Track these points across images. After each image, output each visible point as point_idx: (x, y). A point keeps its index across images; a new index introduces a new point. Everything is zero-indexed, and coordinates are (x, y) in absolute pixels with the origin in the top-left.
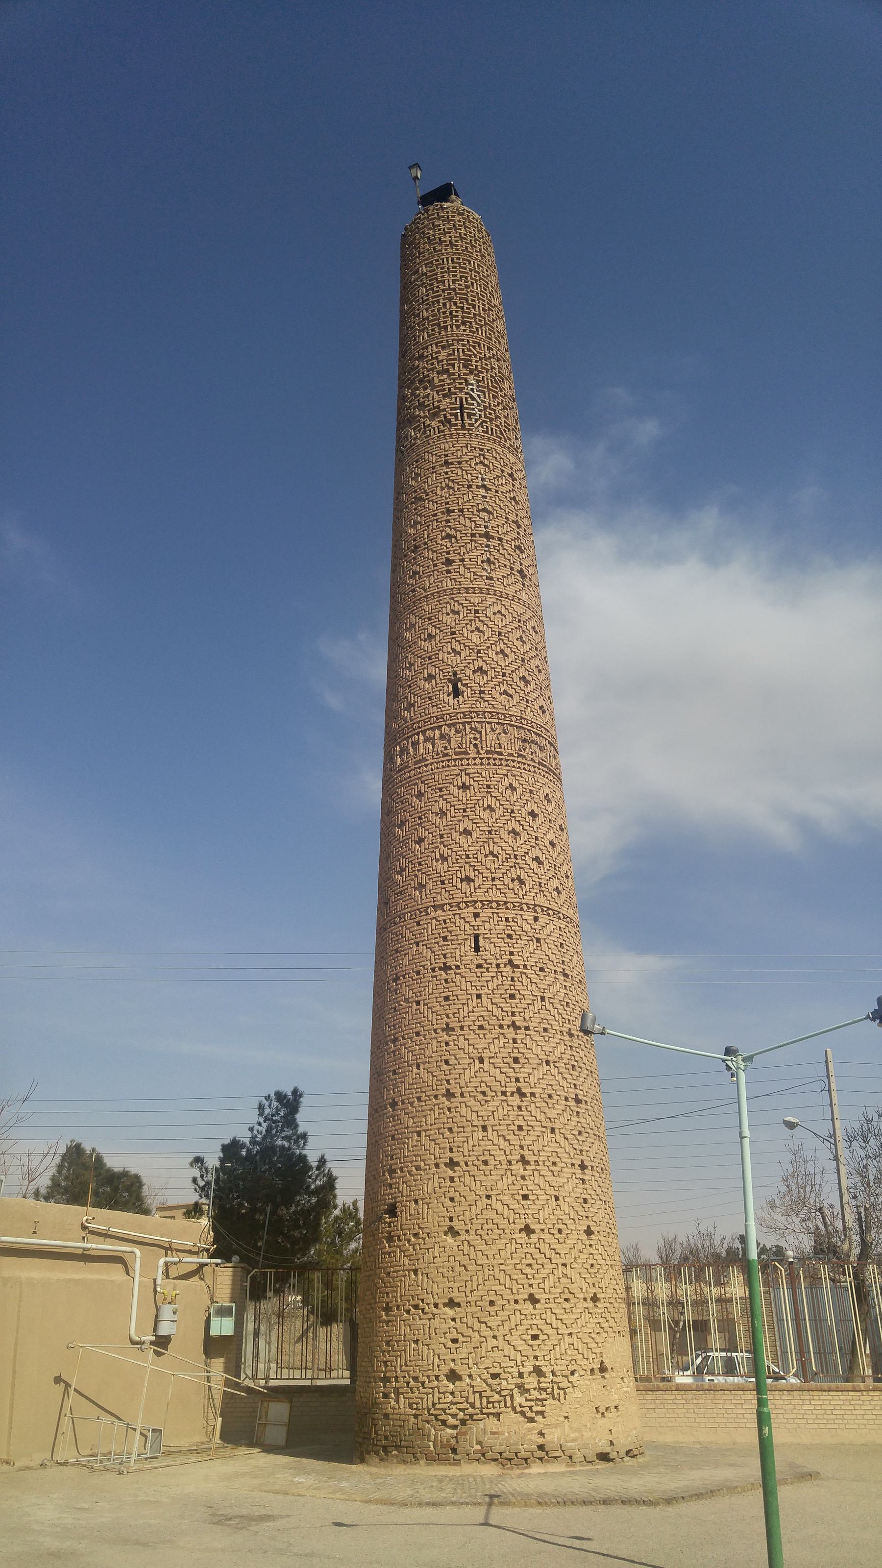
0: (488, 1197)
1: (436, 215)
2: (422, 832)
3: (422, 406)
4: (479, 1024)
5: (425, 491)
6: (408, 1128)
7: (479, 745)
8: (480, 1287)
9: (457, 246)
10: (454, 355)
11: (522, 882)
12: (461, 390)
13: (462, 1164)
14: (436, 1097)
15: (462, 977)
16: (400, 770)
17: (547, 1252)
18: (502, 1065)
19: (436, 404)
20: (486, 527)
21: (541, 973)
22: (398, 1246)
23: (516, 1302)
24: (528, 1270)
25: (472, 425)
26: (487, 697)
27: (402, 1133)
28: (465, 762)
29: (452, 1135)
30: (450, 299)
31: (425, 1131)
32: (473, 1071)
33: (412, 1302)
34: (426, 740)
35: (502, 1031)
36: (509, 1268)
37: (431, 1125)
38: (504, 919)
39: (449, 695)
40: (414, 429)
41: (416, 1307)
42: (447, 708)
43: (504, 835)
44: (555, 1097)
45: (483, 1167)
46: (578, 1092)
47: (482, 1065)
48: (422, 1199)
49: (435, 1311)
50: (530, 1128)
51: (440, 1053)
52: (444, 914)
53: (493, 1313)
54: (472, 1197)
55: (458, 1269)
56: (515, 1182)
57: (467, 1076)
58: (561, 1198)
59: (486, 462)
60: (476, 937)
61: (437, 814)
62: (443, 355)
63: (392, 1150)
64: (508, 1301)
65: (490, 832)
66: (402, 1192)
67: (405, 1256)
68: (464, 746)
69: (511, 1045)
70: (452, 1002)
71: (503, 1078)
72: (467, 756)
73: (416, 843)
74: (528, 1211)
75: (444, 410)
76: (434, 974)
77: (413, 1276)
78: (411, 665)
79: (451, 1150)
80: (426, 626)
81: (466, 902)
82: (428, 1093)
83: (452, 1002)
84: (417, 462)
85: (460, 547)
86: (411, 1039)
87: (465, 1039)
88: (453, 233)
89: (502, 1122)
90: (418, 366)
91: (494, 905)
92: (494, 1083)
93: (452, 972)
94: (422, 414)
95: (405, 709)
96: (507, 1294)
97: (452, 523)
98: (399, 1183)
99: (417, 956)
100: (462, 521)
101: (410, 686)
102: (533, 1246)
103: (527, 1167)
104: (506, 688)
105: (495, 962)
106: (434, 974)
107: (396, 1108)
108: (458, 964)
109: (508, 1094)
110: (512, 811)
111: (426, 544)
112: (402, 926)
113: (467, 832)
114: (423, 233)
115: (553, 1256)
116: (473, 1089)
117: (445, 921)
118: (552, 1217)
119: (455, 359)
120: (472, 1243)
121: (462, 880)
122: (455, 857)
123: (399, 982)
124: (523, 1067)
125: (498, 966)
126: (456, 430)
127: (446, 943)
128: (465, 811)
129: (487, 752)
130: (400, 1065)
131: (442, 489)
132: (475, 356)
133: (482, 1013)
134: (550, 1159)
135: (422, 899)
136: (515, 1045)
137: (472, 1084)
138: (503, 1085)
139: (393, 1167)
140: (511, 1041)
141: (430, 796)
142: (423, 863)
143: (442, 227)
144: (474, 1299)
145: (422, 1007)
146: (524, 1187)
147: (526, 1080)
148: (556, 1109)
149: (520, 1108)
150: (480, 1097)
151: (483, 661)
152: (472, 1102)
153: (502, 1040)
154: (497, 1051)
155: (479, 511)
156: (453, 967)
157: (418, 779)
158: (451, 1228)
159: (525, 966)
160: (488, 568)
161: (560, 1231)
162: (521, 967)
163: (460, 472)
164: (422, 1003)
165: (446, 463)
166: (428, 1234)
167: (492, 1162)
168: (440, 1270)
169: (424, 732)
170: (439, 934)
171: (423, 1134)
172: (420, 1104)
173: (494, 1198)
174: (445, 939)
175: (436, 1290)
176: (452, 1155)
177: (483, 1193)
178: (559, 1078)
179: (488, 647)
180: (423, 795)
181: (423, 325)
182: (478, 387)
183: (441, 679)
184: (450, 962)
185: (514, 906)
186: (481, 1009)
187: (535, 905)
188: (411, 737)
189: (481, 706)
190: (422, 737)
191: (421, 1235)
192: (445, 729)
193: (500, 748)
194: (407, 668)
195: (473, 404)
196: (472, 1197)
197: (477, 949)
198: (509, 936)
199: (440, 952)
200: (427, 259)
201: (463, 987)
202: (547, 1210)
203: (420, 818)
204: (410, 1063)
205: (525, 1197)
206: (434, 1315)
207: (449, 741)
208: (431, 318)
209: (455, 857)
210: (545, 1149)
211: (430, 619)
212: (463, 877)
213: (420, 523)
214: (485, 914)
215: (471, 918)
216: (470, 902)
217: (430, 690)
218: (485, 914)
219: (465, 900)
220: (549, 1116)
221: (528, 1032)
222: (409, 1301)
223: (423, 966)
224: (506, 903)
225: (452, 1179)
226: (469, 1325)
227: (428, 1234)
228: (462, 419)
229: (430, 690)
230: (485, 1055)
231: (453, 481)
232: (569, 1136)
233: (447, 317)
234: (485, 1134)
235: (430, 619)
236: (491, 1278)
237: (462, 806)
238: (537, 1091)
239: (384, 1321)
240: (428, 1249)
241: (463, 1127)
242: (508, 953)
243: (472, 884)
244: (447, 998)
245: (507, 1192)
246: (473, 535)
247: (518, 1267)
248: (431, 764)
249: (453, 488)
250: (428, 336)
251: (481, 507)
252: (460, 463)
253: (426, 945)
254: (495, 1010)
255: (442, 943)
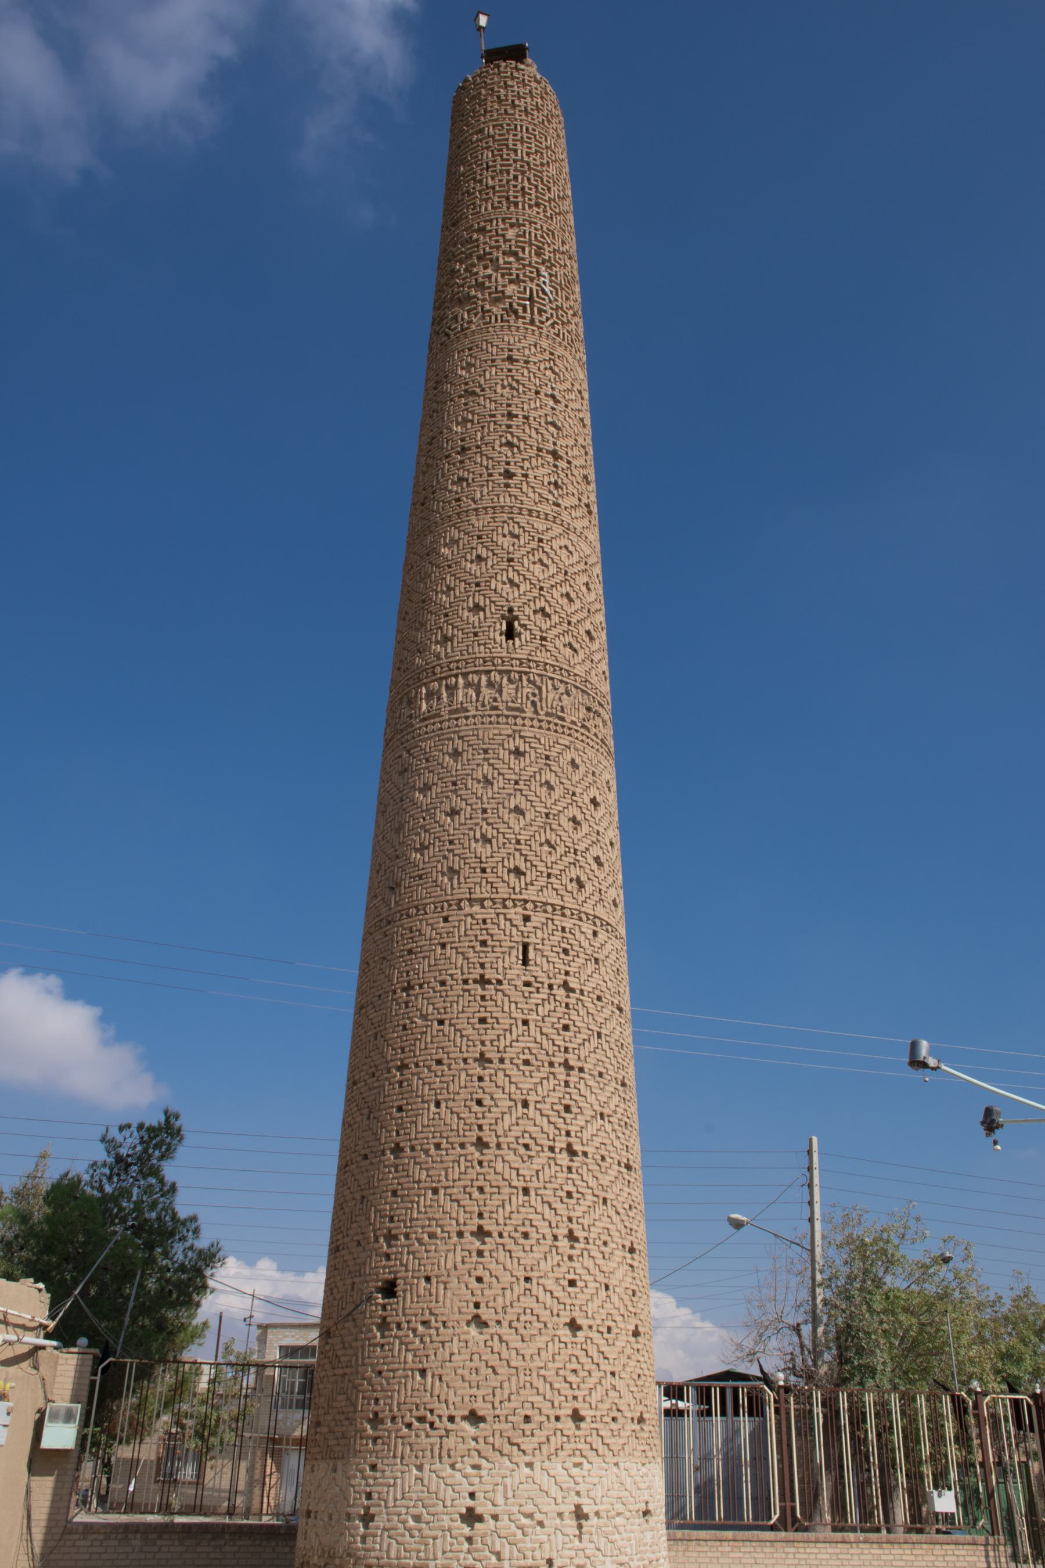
0: (527, 1279)
1: (509, 74)
2: (457, 803)
3: (480, 286)
4: (525, 1057)
5: (480, 386)
6: (419, 1182)
7: (538, 704)
8: (512, 1397)
9: (530, 194)
10: (524, 237)
11: (581, 885)
12: (532, 280)
13: (495, 1235)
14: (462, 1146)
15: (505, 995)
16: (425, 719)
17: (595, 1355)
18: (551, 1113)
19: (500, 288)
20: (555, 444)
21: (598, 1003)
22: (396, 1337)
23: (557, 1418)
24: (572, 1378)
25: (542, 322)
26: (550, 646)
27: (409, 1189)
28: (519, 721)
29: (483, 1196)
30: (523, 173)
31: (446, 1188)
32: (514, 1116)
33: (415, 1413)
34: (468, 685)
35: (552, 1070)
36: (550, 1374)
37: (454, 1181)
38: (560, 928)
39: (501, 634)
40: (469, 311)
41: (421, 1419)
42: (499, 649)
43: (564, 821)
44: (608, 1160)
45: (521, 1241)
46: (631, 1157)
47: (525, 1111)
48: (437, 1276)
49: (450, 1426)
50: (580, 1196)
51: (470, 1090)
52: (483, 910)
53: (528, 1433)
54: (506, 1278)
55: (484, 1371)
56: (561, 1263)
57: (506, 1123)
58: (611, 1287)
59: (556, 370)
60: (525, 947)
61: (479, 782)
62: (511, 234)
63: (391, 1209)
64: (548, 1417)
65: (547, 815)
66: (406, 1266)
67: (407, 1350)
68: (519, 701)
69: (562, 1089)
70: (489, 1026)
71: (551, 1130)
72: (523, 715)
73: (447, 814)
74: (574, 1302)
75: (510, 297)
76: (466, 987)
77: (418, 1378)
78: (449, 588)
79: (480, 1215)
80: (474, 545)
81: (513, 900)
82: (450, 1140)
83: (489, 1026)
84: (470, 349)
85: (523, 460)
86: (429, 1068)
87: (506, 1075)
88: (529, 100)
89: (548, 1185)
90: (477, 240)
91: (549, 908)
92: (540, 1135)
93: (492, 987)
94: (480, 296)
95: (437, 642)
96: (546, 1407)
97: (514, 373)
98: (401, 1253)
99: (443, 961)
100: (527, 430)
101: (446, 615)
102: (579, 1346)
103: (576, 1245)
104: (571, 640)
105: (547, 981)
106: (466, 987)
107: (402, 1154)
108: (500, 977)
109: (557, 1150)
110: (574, 794)
111: (478, 447)
112: (421, 921)
113: (518, 811)
114: (492, 89)
115: (601, 1361)
116: (513, 1140)
117: (484, 921)
118: (601, 1310)
119: (525, 242)
120: (504, 1338)
121: (509, 871)
122: (501, 840)
123: (411, 992)
124: (575, 1119)
125: (551, 987)
126: (524, 323)
127: (485, 949)
128: (517, 783)
129: (547, 714)
130: (410, 1101)
131: (503, 387)
132: (549, 246)
133: (529, 1045)
134: (602, 1236)
135: (453, 888)
136: (568, 1090)
137: (512, 1133)
138: (551, 1137)
139: (393, 1232)
140: (563, 1084)
141: (470, 757)
142: (456, 842)
143: (515, 88)
144: (504, 1412)
145: (446, 1028)
146: (572, 1271)
147: (579, 1134)
148: (610, 1175)
149: (569, 1169)
150: (522, 1150)
151: (546, 601)
152: (510, 1157)
153: (552, 1081)
154: (545, 1094)
155: (547, 423)
156: (494, 981)
157: (455, 732)
158: (477, 1317)
159: (582, 992)
160: (555, 492)
161: (609, 1330)
162: (578, 991)
163: (526, 373)
164: (447, 1022)
165: (510, 359)
166: (444, 1323)
167: (533, 1235)
168: (460, 1371)
169: (465, 675)
170: (476, 936)
171: (442, 1192)
172: (439, 1152)
173: (534, 1281)
174: (484, 943)
175: (452, 1398)
176: (481, 1222)
177: (521, 1274)
178: (613, 1136)
179: (552, 586)
180: (460, 754)
181: (487, 194)
182: (551, 281)
183: (492, 613)
184: (490, 974)
185: (572, 914)
186: (527, 1038)
187: (595, 917)
188: (446, 678)
189: (541, 656)
190: (461, 681)
191: (433, 1323)
192: (495, 677)
193: (563, 711)
194: (443, 592)
195: (544, 299)
196: (506, 1278)
197: (525, 962)
198: (566, 951)
199: (475, 960)
200: (495, 120)
201: (506, 1009)
202: (597, 1302)
203: (454, 784)
204: (426, 1098)
205: (572, 1283)
206: (447, 1431)
207: (500, 691)
208: (497, 188)
209: (501, 840)
210: (597, 1223)
211: (480, 537)
212: (512, 867)
213: (472, 421)
214: (538, 918)
215: (519, 921)
216: (520, 900)
217: (476, 624)
218: (537, 919)
219: (513, 896)
220: (601, 1182)
221: (582, 1075)
222: (411, 1411)
223: (451, 975)
224: (563, 908)
225: (480, 1253)
226: (496, 1447)
227: (444, 1323)
228: (532, 313)
229: (476, 624)
230: (532, 1098)
231: (517, 381)
232: (621, 1211)
233: (517, 192)
234: (526, 1198)
235: (480, 537)
236: (528, 1385)
237: (514, 777)
238: (590, 1150)
239: (368, 1438)
240: (443, 1343)
241: (498, 1187)
242: (563, 972)
243: (522, 877)
244: (483, 1021)
245: (550, 1275)
246: (539, 450)
247: (561, 1372)
248: (474, 717)
249: (518, 390)
250: (493, 208)
251: (550, 419)
252: (527, 362)
253: (456, 948)
254: (545, 1042)
255: (478, 948)
